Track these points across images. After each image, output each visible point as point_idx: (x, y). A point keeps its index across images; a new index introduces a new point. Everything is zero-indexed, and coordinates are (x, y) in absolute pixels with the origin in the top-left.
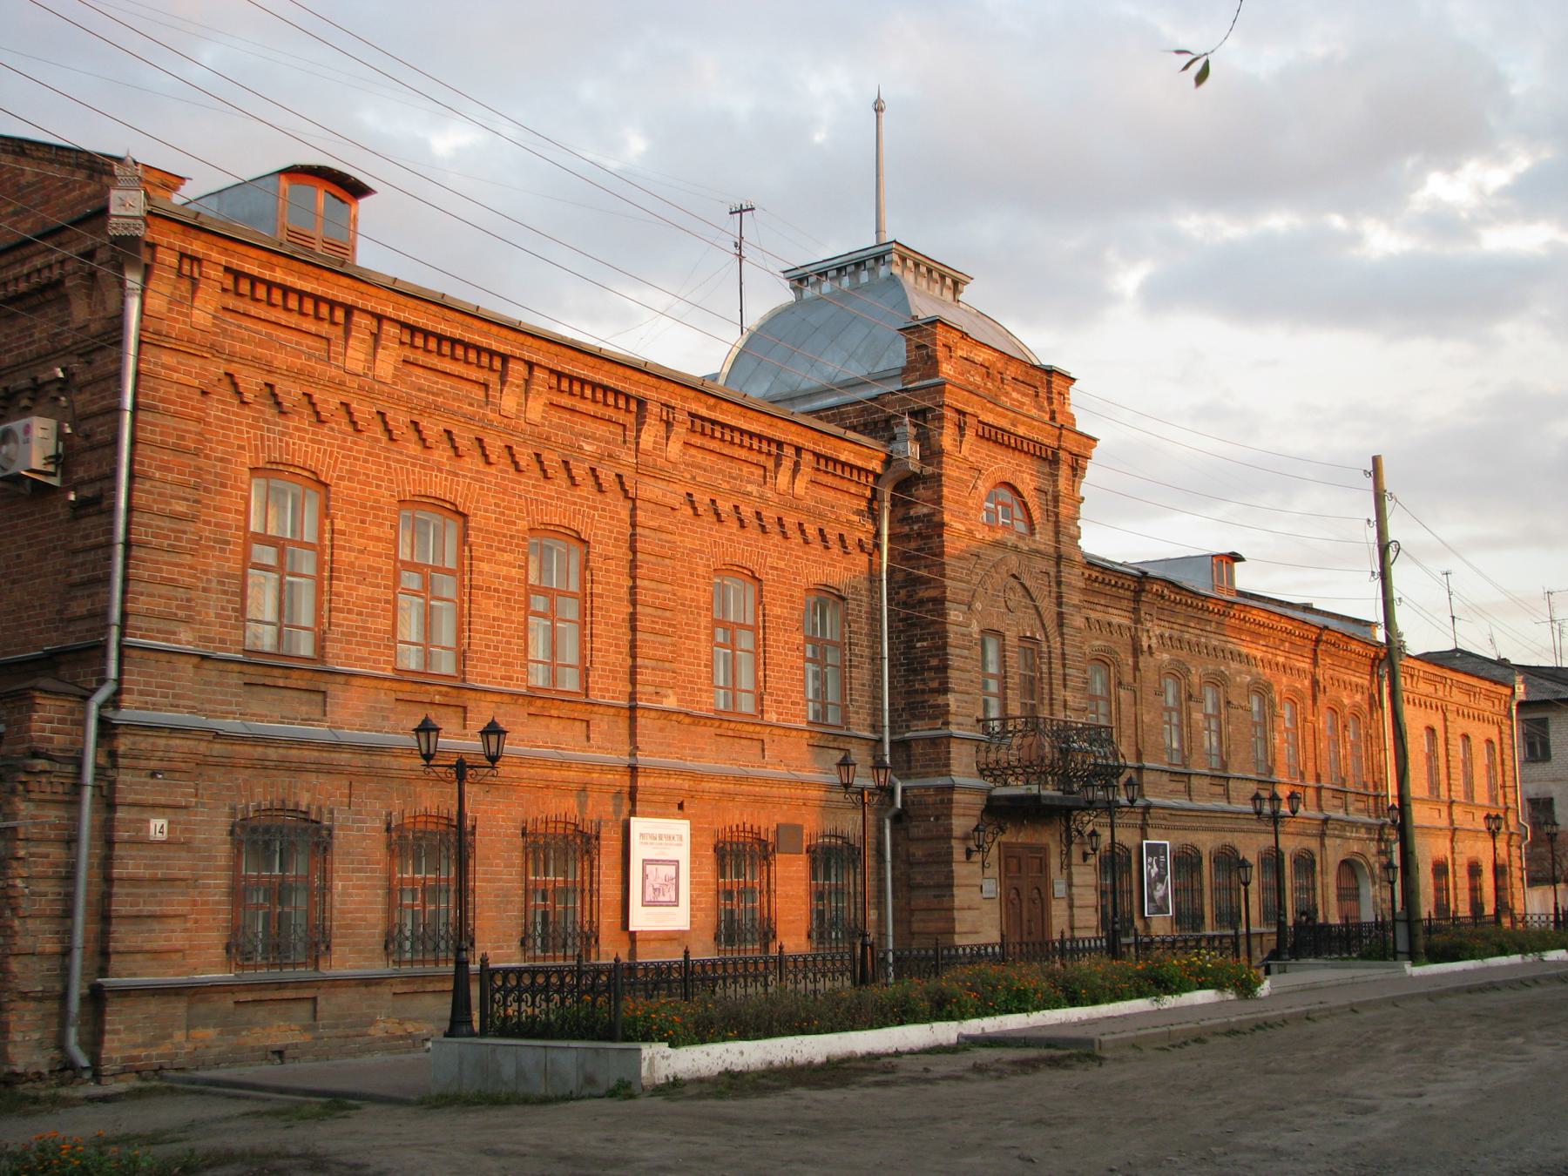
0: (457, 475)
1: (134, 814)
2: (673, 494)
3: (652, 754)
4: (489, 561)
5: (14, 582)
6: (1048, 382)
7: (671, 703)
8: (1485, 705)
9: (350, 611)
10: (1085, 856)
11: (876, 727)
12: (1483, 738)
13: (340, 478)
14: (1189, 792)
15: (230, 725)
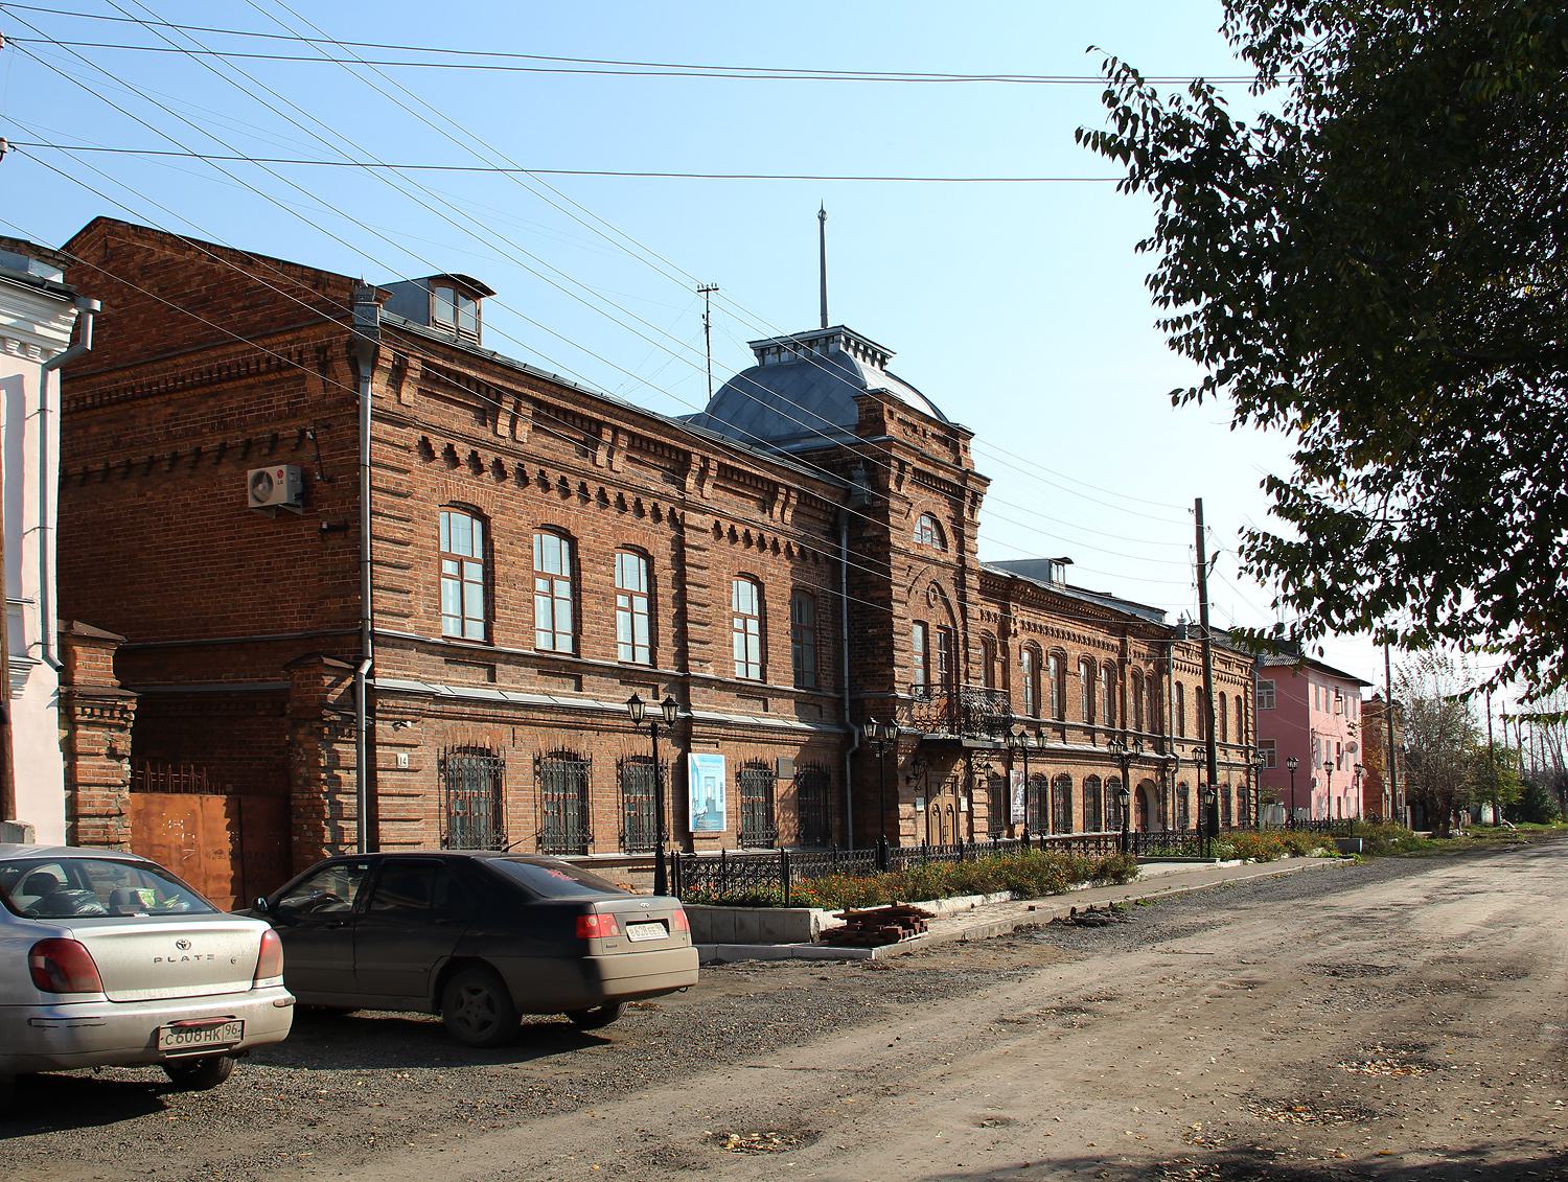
0: (569, 509)
1: (387, 750)
2: (707, 521)
3: (701, 709)
4: (592, 571)
5: (266, 581)
6: (955, 437)
7: (710, 674)
8: (1237, 671)
9: (506, 608)
10: (908, 780)
11: (838, 689)
12: (1234, 696)
13: (496, 512)
14: (1093, 740)
15: (443, 690)
